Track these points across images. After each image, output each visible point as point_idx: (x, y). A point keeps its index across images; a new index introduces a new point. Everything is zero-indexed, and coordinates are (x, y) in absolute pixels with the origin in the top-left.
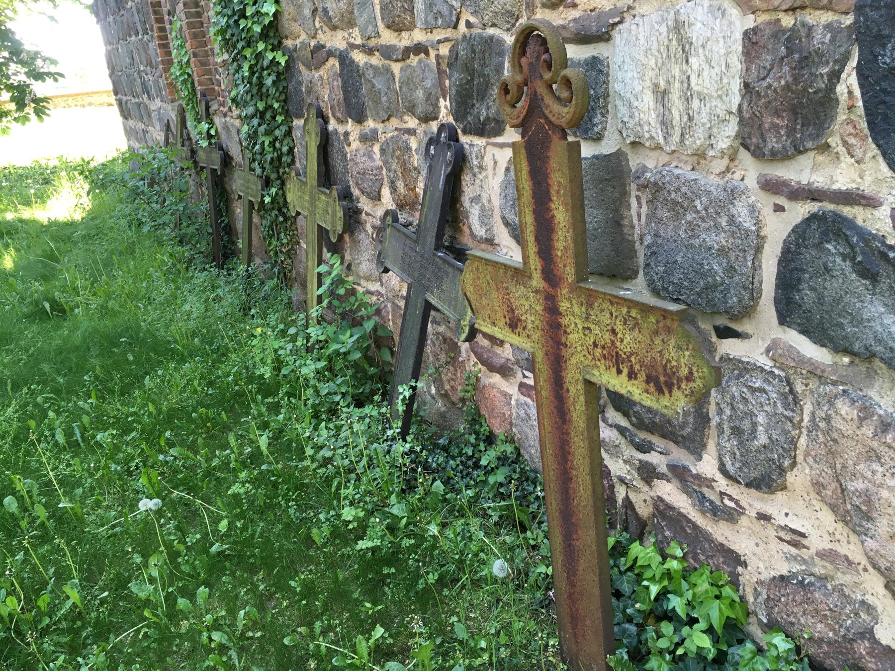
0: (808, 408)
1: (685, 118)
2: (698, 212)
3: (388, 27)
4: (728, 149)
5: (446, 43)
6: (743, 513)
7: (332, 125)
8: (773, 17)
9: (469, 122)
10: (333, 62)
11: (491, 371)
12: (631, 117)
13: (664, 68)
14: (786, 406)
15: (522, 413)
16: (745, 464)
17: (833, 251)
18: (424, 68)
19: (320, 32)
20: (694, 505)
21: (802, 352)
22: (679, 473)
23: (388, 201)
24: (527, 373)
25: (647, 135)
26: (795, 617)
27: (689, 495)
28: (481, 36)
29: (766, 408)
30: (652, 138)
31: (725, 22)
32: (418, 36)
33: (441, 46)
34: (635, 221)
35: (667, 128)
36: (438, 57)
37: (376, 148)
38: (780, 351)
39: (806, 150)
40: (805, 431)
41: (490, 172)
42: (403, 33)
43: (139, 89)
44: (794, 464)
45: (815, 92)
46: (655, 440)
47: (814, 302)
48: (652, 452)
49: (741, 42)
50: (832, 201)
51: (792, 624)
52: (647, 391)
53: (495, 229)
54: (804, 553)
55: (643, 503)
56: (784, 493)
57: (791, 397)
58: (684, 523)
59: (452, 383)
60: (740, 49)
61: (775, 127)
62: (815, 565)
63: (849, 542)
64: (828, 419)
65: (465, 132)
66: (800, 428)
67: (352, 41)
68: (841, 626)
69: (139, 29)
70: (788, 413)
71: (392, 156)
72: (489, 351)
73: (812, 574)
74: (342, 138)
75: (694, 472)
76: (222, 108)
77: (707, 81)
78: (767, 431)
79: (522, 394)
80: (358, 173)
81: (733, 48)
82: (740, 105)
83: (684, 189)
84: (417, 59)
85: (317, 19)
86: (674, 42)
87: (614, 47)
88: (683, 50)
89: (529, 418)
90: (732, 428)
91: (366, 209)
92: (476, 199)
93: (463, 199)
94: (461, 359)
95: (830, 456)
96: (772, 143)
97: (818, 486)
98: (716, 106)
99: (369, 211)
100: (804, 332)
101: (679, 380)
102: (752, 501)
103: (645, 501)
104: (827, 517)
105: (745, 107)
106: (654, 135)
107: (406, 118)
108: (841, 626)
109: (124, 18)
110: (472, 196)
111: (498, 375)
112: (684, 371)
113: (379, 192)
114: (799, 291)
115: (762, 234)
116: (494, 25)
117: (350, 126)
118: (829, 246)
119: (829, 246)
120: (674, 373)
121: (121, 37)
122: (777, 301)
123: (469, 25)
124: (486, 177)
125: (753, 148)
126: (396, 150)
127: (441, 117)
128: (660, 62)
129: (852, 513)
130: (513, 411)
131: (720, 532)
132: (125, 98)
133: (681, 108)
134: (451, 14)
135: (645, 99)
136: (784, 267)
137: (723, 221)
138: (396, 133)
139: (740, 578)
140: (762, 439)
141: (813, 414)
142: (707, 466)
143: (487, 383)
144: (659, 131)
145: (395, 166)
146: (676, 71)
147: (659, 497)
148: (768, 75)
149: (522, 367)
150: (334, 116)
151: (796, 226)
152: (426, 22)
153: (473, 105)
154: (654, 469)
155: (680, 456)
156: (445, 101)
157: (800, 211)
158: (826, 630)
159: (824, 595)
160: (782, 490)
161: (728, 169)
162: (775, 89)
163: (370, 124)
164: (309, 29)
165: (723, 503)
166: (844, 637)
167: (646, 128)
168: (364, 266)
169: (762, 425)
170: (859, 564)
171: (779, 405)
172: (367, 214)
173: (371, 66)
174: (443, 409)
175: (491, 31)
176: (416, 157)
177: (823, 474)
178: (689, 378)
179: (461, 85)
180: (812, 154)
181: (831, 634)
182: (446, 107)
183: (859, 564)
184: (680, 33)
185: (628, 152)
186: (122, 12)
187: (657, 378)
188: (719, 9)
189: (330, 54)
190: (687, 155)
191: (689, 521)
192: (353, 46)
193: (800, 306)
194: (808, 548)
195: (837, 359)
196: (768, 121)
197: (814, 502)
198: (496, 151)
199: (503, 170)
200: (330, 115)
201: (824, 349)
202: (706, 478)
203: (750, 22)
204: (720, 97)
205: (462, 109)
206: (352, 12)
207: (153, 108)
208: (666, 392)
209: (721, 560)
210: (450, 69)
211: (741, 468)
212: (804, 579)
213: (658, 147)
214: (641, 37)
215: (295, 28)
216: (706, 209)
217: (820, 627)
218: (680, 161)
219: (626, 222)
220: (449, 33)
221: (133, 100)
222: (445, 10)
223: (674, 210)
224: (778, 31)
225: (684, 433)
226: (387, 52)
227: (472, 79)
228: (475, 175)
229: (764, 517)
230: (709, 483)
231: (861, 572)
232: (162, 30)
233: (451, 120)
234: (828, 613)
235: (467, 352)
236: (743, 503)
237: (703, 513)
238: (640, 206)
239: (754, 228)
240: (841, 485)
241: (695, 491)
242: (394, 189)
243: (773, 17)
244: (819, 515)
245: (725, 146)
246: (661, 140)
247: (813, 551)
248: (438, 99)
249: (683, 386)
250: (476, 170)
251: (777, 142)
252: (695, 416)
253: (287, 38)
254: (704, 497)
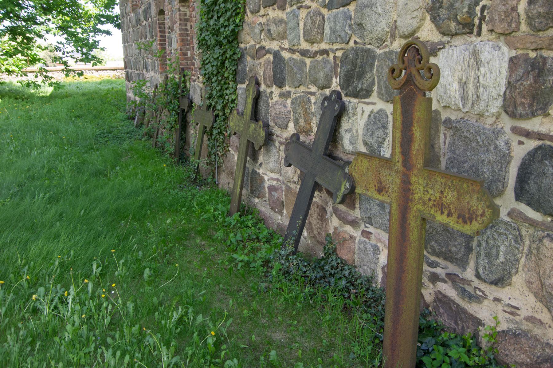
0: (527, 243)
1: (475, 96)
2: (478, 142)
3: (307, 41)
4: (496, 113)
5: (341, 51)
6: (486, 298)
7: (263, 87)
8: (525, 52)
9: (350, 91)
10: (270, 57)
11: (345, 224)
12: (445, 93)
13: (466, 72)
14: (516, 241)
15: (362, 247)
16: (491, 272)
17: (549, 164)
18: (326, 62)
19: (263, 41)
20: (458, 295)
21: (527, 215)
22: (452, 278)
23: (291, 129)
24: (367, 225)
25: (453, 103)
26: (509, 351)
27: (456, 289)
28: (362, 48)
29: (505, 243)
30: (456, 104)
31: (500, 53)
32: (324, 46)
33: (337, 52)
34: (442, 146)
35: (464, 100)
36: (335, 57)
37: (289, 101)
38: (515, 214)
39: (538, 115)
40: (524, 255)
41: (359, 116)
42: (315, 44)
43: (141, 66)
44: (517, 272)
45: (545, 88)
46: (440, 261)
47: (536, 189)
48: (438, 268)
49: (507, 62)
50: (549, 140)
51: (507, 355)
52: (458, 223)
53: (358, 146)
54: (517, 318)
55: (429, 295)
56: (509, 287)
57: (519, 238)
58: (452, 304)
59: (319, 230)
60: (507, 66)
61: (523, 104)
62: (522, 325)
63: (542, 312)
64: (538, 249)
65: (346, 95)
66: (522, 253)
67: (283, 46)
68: (534, 356)
69: (148, 35)
70: (517, 246)
71: (299, 106)
72: (345, 213)
73: (521, 329)
74: (268, 95)
75: (461, 277)
76: (193, 77)
77: (488, 80)
78: (504, 255)
79: (363, 236)
80: (276, 114)
81: (504, 65)
82: (505, 92)
83: (471, 131)
84: (321, 57)
85: (263, 34)
86: (472, 60)
87: (439, 59)
88: (477, 64)
89: (366, 249)
90: (486, 254)
91: (277, 133)
92: (349, 130)
93: (340, 130)
94: (326, 217)
95: (537, 268)
96: (520, 110)
97: (529, 283)
98: (492, 92)
99: (279, 134)
100: (529, 204)
101: (477, 216)
102: (492, 291)
103: (430, 294)
104: (532, 299)
105: (507, 93)
106: (457, 103)
107: (310, 86)
108: (534, 356)
109: (140, 30)
110: (346, 128)
111: (349, 226)
112: (480, 212)
113: (287, 124)
114: (528, 184)
115: (511, 155)
116: (370, 44)
117: (274, 89)
118: (546, 162)
119: (546, 162)
120: (474, 213)
121: (136, 39)
122: (516, 189)
123: (355, 42)
124: (357, 119)
125: (510, 113)
126: (302, 102)
127: (332, 87)
128: (464, 68)
129: (546, 296)
130: (357, 246)
131: (472, 308)
132: (130, 71)
133: (473, 91)
134: (346, 37)
135: (454, 86)
136: (522, 172)
137: (492, 148)
138: (302, 94)
139: (480, 333)
140: (502, 259)
141: (530, 246)
142: (469, 274)
143: (342, 230)
144: (460, 101)
145: (299, 110)
146: (472, 73)
147: (439, 291)
148: (521, 79)
149: (365, 222)
150: (265, 83)
151: (530, 152)
152: (330, 39)
153: (353, 82)
154: (438, 276)
155: (453, 268)
156: (336, 79)
157: (532, 144)
158: (526, 358)
159: (526, 339)
160: (508, 286)
161: (495, 122)
162: (525, 85)
163: (287, 88)
164: (257, 39)
165: (475, 293)
166: (536, 361)
167: (453, 99)
168: (271, 164)
169: (502, 252)
170: (547, 323)
171: (512, 241)
172: (277, 136)
173: (293, 59)
174: (311, 245)
175: (369, 46)
176: (313, 107)
177: (532, 277)
178: (482, 215)
179: (347, 71)
180: (540, 117)
181: (528, 360)
182: (336, 82)
183: (547, 323)
184: (476, 56)
185: (441, 111)
186: (139, 26)
187: (464, 216)
188: (497, 46)
189: (268, 52)
190: (475, 114)
191: (454, 303)
192: (283, 49)
193: (528, 192)
194: (520, 315)
195: (545, 219)
196: (519, 100)
197: (525, 292)
198: (364, 106)
199: (367, 116)
200: (262, 83)
201: (538, 213)
202: (468, 280)
203: (513, 53)
204: (495, 87)
205: (347, 82)
206: (286, 32)
207: (148, 76)
208: (468, 222)
209: (471, 323)
210: (341, 63)
211: (488, 274)
212: (516, 332)
213: (459, 110)
214: (454, 56)
215: (248, 38)
216: (483, 141)
217: (522, 356)
218: (470, 117)
219: (437, 146)
220: (343, 46)
221: (136, 72)
222: (343, 34)
223: (464, 141)
224: (526, 58)
225: (458, 257)
226: (304, 53)
227: (355, 69)
228: (349, 118)
229: (497, 300)
230: (469, 283)
231: (548, 328)
232: (163, 37)
233: (338, 88)
234: (528, 349)
235: (331, 213)
236: (487, 293)
237: (463, 299)
238: (445, 138)
239: (507, 152)
240: (541, 282)
241: (460, 287)
242: (297, 122)
243: (525, 52)
244: (527, 298)
245: (495, 111)
246: (461, 106)
247: (522, 317)
248: (332, 78)
249: (479, 219)
250: (351, 115)
251: (523, 111)
252: (465, 248)
253: (241, 43)
254: (465, 290)
